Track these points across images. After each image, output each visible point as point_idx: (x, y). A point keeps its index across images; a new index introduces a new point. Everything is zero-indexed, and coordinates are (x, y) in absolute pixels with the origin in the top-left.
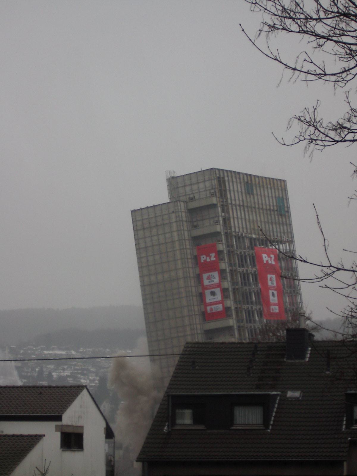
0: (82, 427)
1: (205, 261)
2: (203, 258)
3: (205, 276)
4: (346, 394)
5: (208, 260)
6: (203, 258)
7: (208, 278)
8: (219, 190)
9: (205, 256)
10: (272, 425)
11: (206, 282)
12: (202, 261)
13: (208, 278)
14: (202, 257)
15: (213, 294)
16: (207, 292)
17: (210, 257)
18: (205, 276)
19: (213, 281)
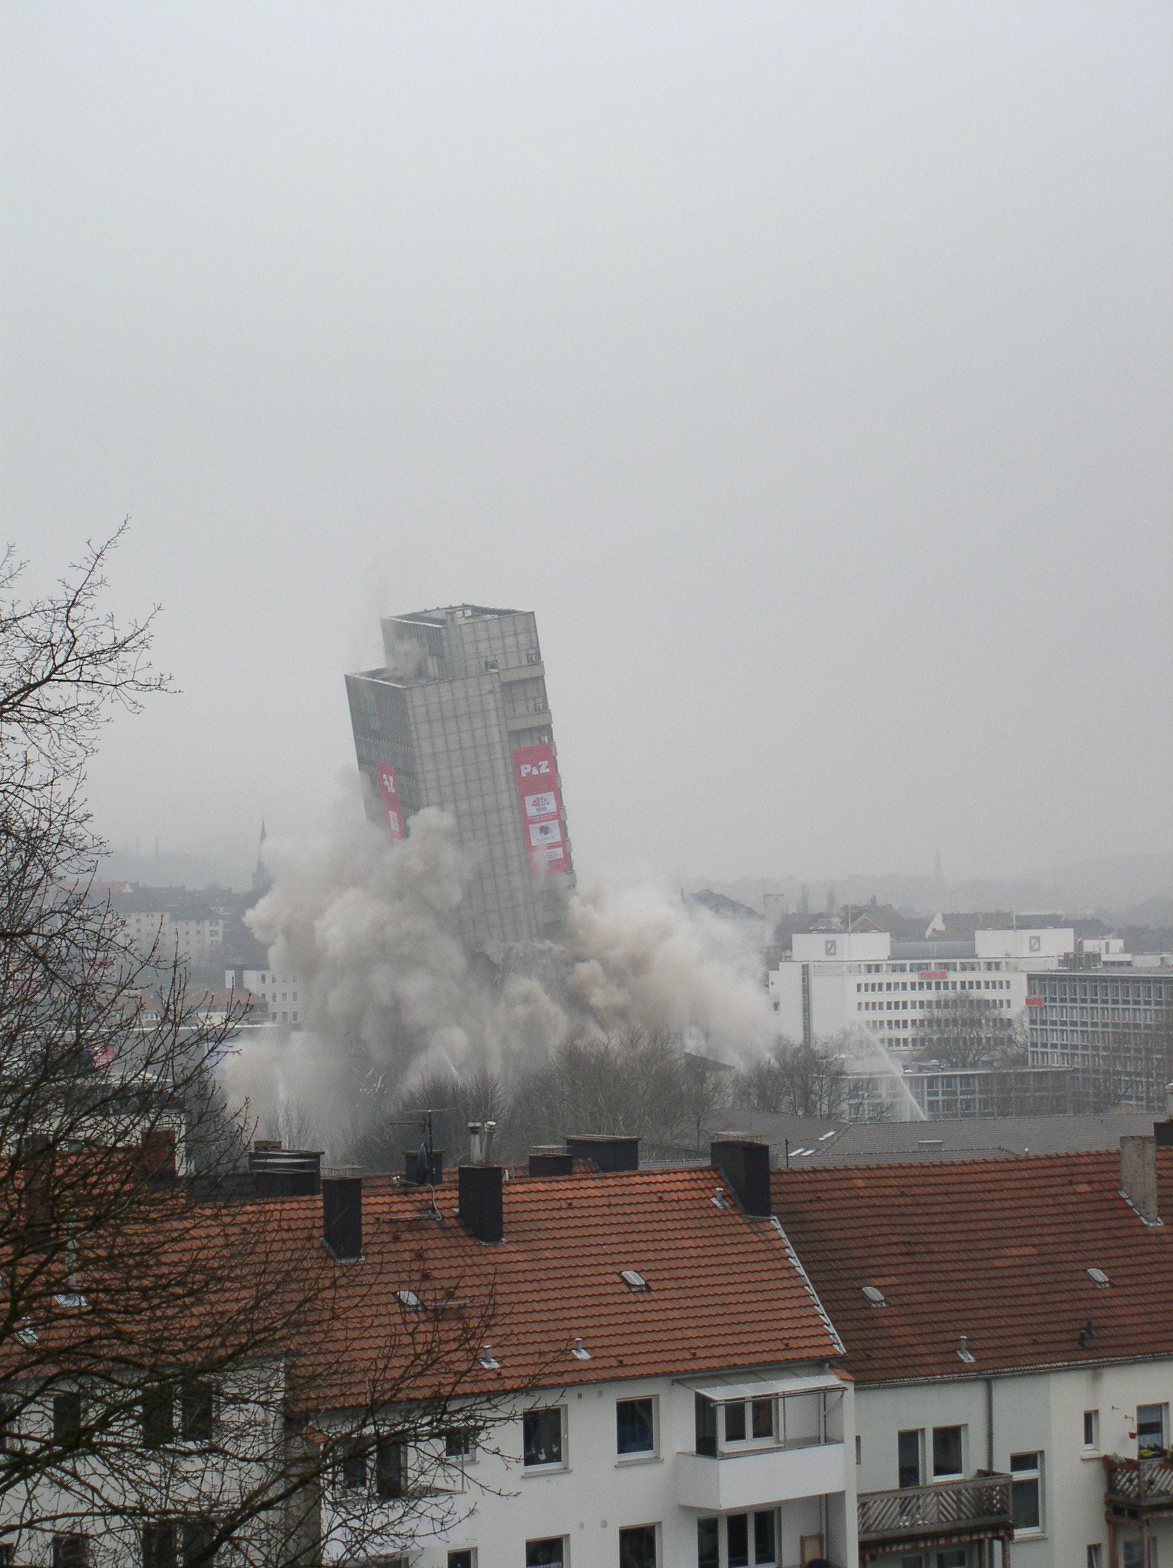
0: (780, 1038)
1: (529, 774)
2: (525, 770)
3: (529, 800)
4: (460, 1169)
5: (535, 772)
6: (525, 770)
7: (536, 803)
8: (776, 1558)
9: (528, 766)
10: (185, 1139)
11: (531, 811)
12: (524, 775)
13: (536, 803)
14: (522, 767)
15: (544, 830)
16: (534, 830)
17: (539, 767)
18: (529, 800)
19: (545, 809)
